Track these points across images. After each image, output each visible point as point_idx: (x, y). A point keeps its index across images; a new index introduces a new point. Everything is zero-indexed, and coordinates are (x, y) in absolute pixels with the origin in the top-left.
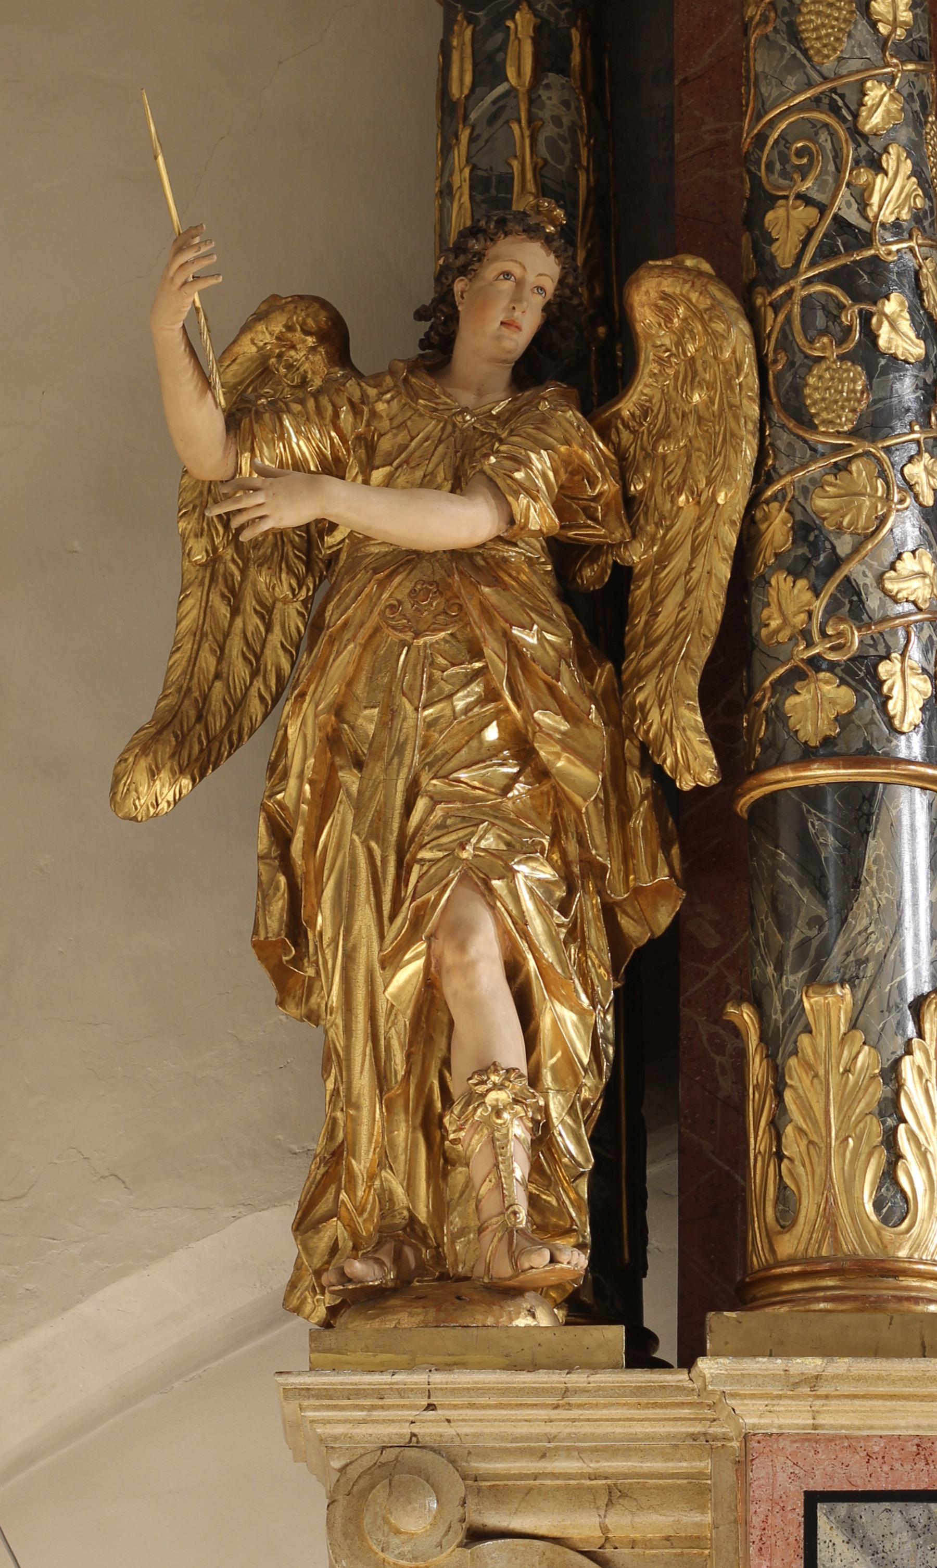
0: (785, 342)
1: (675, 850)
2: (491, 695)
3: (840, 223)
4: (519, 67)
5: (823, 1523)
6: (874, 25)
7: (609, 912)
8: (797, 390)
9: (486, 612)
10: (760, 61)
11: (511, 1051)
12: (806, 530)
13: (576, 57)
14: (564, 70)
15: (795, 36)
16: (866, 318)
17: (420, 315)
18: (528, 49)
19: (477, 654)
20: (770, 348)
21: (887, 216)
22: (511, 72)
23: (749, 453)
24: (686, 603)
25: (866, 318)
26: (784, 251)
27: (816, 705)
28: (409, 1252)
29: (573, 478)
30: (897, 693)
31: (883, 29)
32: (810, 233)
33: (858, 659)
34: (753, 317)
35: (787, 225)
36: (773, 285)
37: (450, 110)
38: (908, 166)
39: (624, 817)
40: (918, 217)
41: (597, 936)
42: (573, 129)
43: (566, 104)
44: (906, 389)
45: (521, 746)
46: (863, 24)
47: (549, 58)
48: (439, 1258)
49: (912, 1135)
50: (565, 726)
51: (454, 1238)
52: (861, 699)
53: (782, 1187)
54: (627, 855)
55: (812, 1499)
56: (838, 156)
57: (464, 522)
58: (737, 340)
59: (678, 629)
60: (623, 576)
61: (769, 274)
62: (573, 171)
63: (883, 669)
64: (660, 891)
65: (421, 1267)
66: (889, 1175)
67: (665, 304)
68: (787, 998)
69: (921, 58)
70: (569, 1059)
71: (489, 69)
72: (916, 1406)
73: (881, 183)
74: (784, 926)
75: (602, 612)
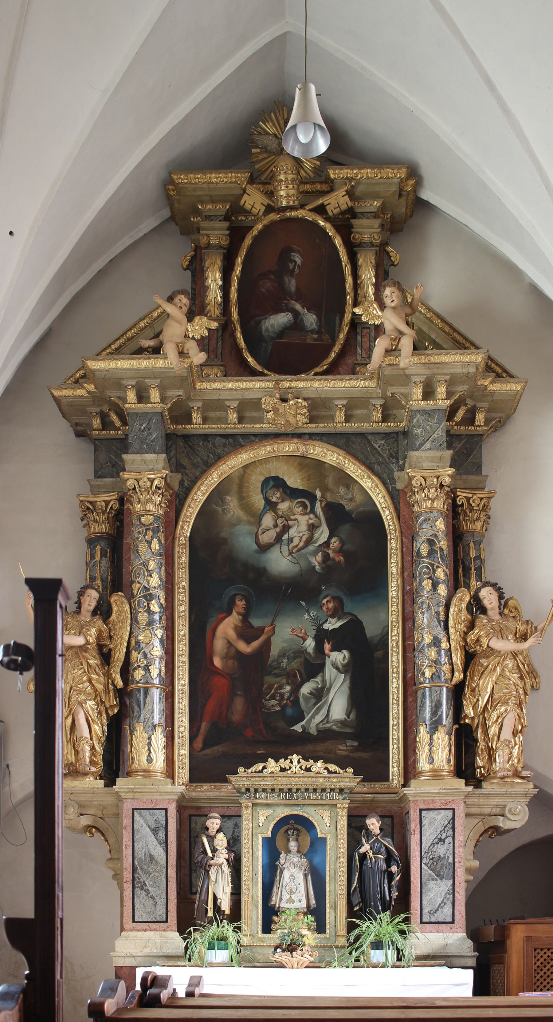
0: (135, 609)
1: (118, 699)
2: (85, 672)
3: (145, 587)
4: (98, 558)
5: (135, 813)
6: (151, 550)
7: (106, 709)
8: (136, 617)
9: (83, 656)
10: (132, 557)
11: (86, 733)
12: (138, 643)
13: (108, 554)
14: (106, 557)
15: (138, 552)
16: (148, 604)
17: (76, 603)
18: (99, 553)
19: (82, 665)
20: (133, 609)
21: (153, 585)
22: (96, 557)
23: (129, 628)
24: (119, 656)
25: (148, 604)
26: (135, 592)
27: (139, 674)
28: (71, 768)
29: (100, 632)
30: (152, 672)
31: (153, 551)
32: (139, 588)
33: (146, 666)
34: (130, 605)
35: (136, 586)
36: (134, 598)
37: (87, 564)
38: (157, 576)
39: (109, 692)
40: (159, 586)
41: (104, 714)
42: (108, 568)
43: (106, 563)
44: (157, 617)
45: (90, 681)
46: (149, 549)
47: (103, 555)
48: (76, 768)
49: (153, 749)
50: (97, 677)
51: (79, 766)
52: (146, 673)
53: (132, 757)
54: (109, 700)
55: (134, 809)
56: (144, 574)
57: (79, 641)
58: (127, 608)
59: (118, 660)
60: (110, 650)
61: (133, 596)
62: (107, 576)
63: (150, 668)
64: (114, 706)
65: (73, 770)
66: (149, 755)
67: (118, 602)
68: (133, 725)
69: (161, 556)
70: (97, 735)
71: (93, 557)
72: (151, 794)
73: (152, 579)
74: (133, 713)
75: (106, 657)
